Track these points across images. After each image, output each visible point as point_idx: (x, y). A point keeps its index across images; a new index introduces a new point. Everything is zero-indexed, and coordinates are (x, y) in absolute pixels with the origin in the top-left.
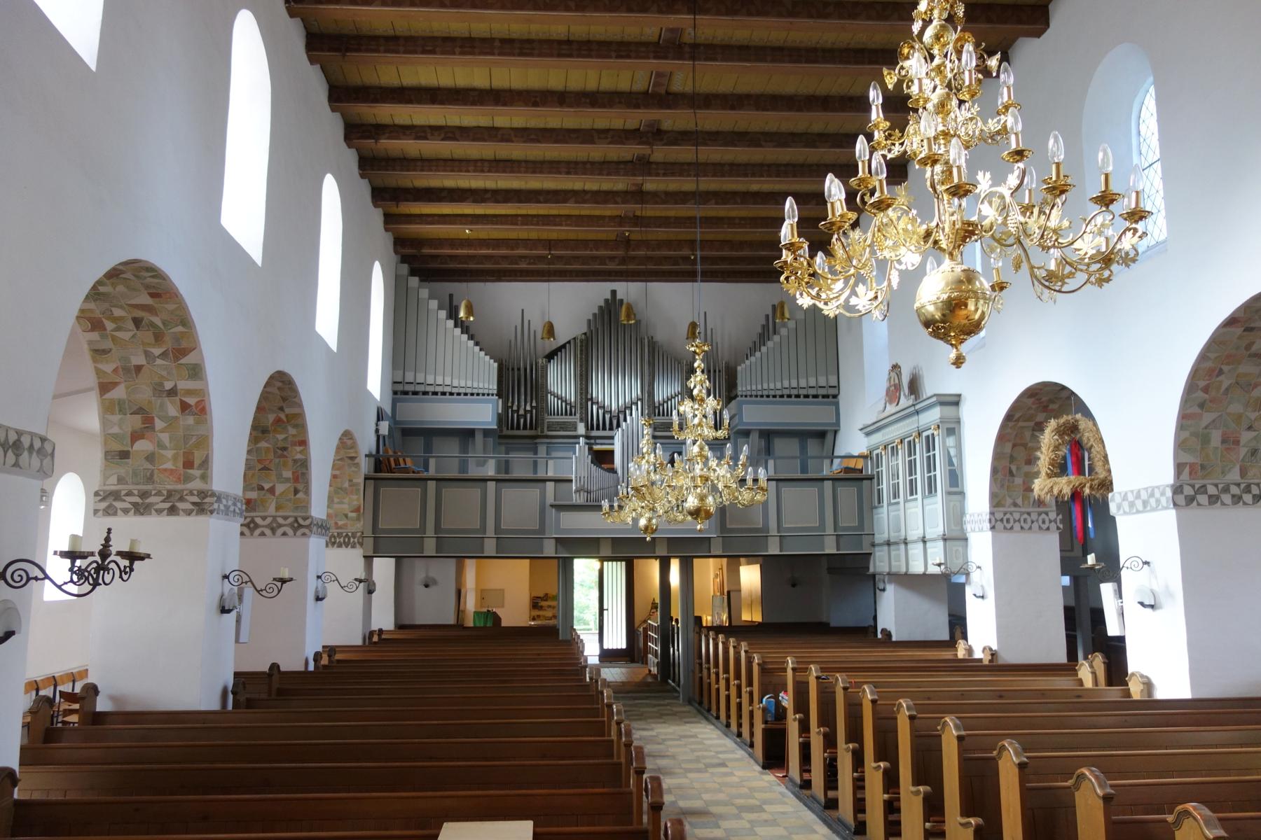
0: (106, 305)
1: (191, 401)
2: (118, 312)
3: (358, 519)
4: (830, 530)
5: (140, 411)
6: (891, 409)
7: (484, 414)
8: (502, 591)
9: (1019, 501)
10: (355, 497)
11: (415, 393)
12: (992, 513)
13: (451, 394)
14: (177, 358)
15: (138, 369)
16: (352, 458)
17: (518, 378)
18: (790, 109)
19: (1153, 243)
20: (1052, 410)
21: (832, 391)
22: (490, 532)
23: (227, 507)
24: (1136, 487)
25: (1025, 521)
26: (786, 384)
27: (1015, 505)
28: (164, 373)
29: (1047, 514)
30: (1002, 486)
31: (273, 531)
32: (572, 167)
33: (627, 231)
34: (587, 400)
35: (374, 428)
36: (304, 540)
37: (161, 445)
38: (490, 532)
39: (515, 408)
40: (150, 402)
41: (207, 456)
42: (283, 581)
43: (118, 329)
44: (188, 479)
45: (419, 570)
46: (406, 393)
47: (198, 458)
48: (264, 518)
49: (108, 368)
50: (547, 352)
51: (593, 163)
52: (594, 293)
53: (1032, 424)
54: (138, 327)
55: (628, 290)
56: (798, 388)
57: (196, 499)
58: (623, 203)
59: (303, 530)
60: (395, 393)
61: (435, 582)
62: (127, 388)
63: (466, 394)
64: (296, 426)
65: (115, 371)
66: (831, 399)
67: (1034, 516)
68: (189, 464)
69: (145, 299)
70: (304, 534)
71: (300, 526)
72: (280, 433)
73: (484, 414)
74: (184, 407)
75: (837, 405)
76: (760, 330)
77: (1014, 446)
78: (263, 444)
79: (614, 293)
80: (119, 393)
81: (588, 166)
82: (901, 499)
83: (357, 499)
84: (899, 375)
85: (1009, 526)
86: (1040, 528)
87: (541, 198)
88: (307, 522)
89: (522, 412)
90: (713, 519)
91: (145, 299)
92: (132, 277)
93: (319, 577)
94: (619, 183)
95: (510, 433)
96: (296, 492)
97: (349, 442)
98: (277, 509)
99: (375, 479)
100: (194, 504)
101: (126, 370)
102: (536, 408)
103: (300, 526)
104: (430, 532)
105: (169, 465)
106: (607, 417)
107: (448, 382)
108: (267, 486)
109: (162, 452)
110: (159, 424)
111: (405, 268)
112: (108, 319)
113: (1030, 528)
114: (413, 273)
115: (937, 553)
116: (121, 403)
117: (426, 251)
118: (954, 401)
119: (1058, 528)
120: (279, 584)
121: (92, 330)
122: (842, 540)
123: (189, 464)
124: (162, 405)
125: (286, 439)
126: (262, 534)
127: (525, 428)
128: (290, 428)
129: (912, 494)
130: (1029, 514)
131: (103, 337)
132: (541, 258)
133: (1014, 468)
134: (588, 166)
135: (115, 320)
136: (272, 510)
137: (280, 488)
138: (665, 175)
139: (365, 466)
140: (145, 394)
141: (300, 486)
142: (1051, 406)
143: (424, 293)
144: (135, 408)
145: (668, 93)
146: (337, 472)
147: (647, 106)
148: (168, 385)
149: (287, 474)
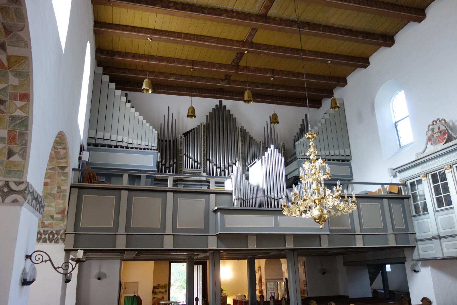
3: (62, 220)
8: (138, 283)
10: (61, 202)
11: (103, 146)
13: (127, 147)
16: (63, 168)
21: (347, 158)
22: (169, 230)
35: (78, 155)
36: (14, 208)
38: (169, 230)
50: (185, 132)
52: (205, 105)
58: (256, 21)
61: (105, 276)
63: (136, 148)
64: (18, 74)
66: (346, 162)
70: (15, 201)
71: (11, 191)
75: (350, 165)
76: (300, 127)
83: (62, 203)
88: (22, 187)
90: (327, 222)
93: (28, 257)
96: (10, 154)
97: (62, 152)
99: (79, 188)
103: (11, 191)
111: (100, 70)
128: (11, 76)
139: (71, 178)
141: (16, 148)
146: (48, 180)
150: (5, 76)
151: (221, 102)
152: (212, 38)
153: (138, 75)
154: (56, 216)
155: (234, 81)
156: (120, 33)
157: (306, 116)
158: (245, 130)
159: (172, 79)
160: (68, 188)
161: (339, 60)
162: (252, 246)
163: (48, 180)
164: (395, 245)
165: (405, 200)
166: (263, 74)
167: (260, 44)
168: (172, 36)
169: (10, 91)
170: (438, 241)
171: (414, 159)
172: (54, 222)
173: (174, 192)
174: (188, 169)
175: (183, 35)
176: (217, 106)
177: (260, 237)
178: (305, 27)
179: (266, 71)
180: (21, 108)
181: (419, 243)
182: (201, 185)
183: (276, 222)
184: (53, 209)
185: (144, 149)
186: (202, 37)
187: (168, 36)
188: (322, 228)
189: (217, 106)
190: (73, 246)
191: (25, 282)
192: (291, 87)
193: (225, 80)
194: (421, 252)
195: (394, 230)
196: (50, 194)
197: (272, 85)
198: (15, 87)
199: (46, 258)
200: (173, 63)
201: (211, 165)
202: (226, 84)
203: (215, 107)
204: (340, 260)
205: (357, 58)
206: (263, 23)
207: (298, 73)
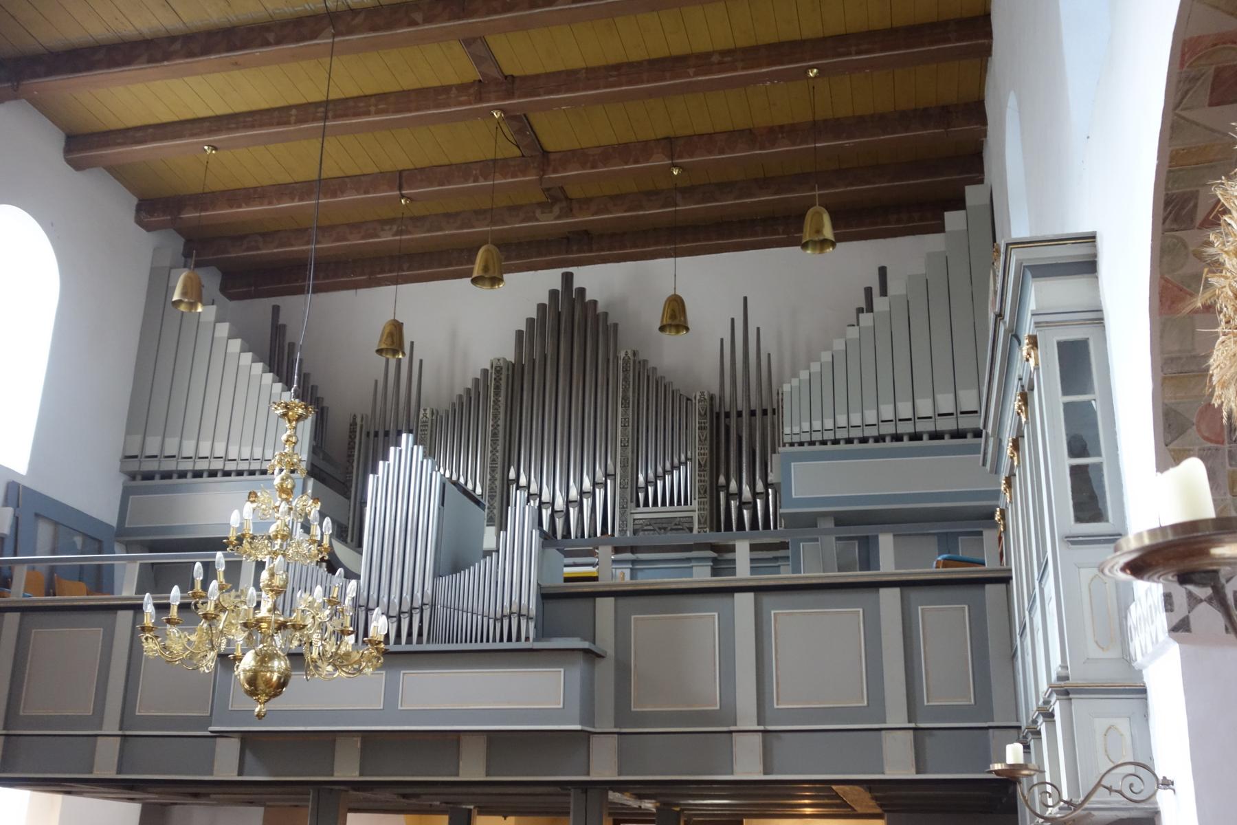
4: (897, 715)
22: (111, 725)
26: (887, 413)
56: (915, 418)
58: (427, 20)
87: (271, 37)
122: (929, 741)
151: (568, 278)
152: (382, 97)
153: (292, 245)
155: (585, 202)
156: (160, 148)
157: (883, 271)
158: (645, 361)
159: (387, 237)
161: (849, 54)
162: (472, 770)
164: (913, 776)
165: (989, 588)
166: (636, 162)
167: (537, 76)
168: (262, 126)
174: (676, 507)
175: (294, 112)
176: (553, 294)
177: (500, 743)
179: (645, 148)
182: (689, 560)
183: (391, 693)
186: (351, 104)
187: (253, 127)
188: (259, 716)
189: (553, 294)
192: (725, 187)
193: (552, 204)
195: (912, 710)
200: (343, 192)
202: (558, 218)
205: (933, 25)
206: (449, 20)
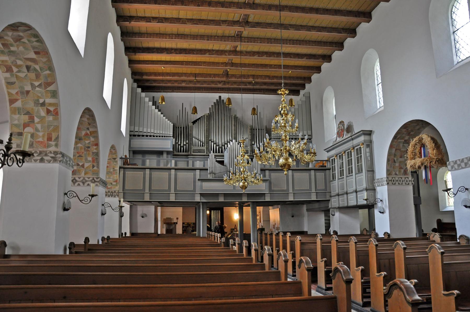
0: (13, 58)
1: (52, 109)
2: (19, 62)
5: (28, 113)
6: (339, 139)
7: (168, 144)
9: (397, 173)
11: (139, 136)
12: (387, 178)
13: (154, 136)
14: (46, 88)
15: (28, 92)
16: (115, 159)
17: (182, 131)
18: (303, 13)
19: (460, 60)
20: (412, 135)
23: (67, 161)
24: (461, 158)
25: (400, 180)
27: (396, 174)
28: (40, 95)
29: (408, 178)
30: (391, 167)
31: (84, 183)
32: (209, 37)
33: (228, 68)
34: (209, 140)
37: (37, 130)
39: (179, 143)
40: (32, 109)
41: (58, 135)
42: (93, 196)
43: (19, 71)
44: (49, 146)
45: (140, 209)
46: (135, 136)
47: (54, 136)
48: (79, 178)
49: (14, 92)
51: (218, 36)
53: (403, 141)
54: (28, 71)
55: (225, 96)
57: (53, 155)
59: (96, 183)
60: (130, 136)
62: (22, 102)
63: (160, 136)
65: (17, 93)
67: (403, 179)
68: (50, 139)
69: (32, 55)
72: (87, 140)
73: (168, 144)
74: (48, 112)
77: (396, 150)
78: (79, 145)
79: (220, 97)
80: (18, 104)
81: (216, 37)
82: (345, 176)
84: (343, 125)
85: (394, 183)
86: (406, 184)
88: (98, 180)
89: (182, 145)
91: (32, 55)
92: (27, 42)
93: (103, 205)
94: (227, 46)
95: (177, 153)
96: (93, 167)
98: (85, 174)
99: (124, 168)
100: (52, 157)
101: (22, 93)
102: (188, 143)
104: (147, 190)
105: (40, 139)
106: (217, 147)
107: (152, 131)
108: (81, 164)
109: (38, 133)
110: (36, 120)
111: (135, 85)
112: (14, 66)
113: (402, 184)
114: (138, 87)
115: (365, 195)
116: (19, 109)
117: (145, 77)
118: (369, 133)
119: (412, 184)
120: (90, 197)
121: (7, 71)
123: (50, 139)
124: (38, 111)
125: (89, 143)
126: (79, 185)
127: (183, 152)
128: (91, 138)
129: (341, 176)
130: (401, 178)
131: (12, 75)
132: (191, 82)
133: (395, 159)
134: (216, 37)
135: (18, 66)
136: (83, 174)
137: (86, 165)
138: (248, 42)
140: (30, 105)
141: (95, 164)
142: (412, 133)
143: (143, 94)
144: (25, 112)
145: (253, 3)
146: (108, 165)
147: (245, 8)
148: (41, 101)
149: (90, 159)
150: (89, 138)
154: (113, 183)
155: (233, 76)
160: (118, 168)
163: (108, 165)
169: (91, 143)
170: (337, 197)
171: (332, 145)
172: (113, 187)
173: (175, 169)
176: (217, 100)
178: (264, 55)
179: (248, 76)
180: (95, 149)
181: (332, 198)
184: (111, 180)
185: (165, 137)
189: (217, 100)
190: (285, 64)
191: (103, 214)
194: (333, 204)
196: (109, 172)
197: (254, 85)
198: (93, 141)
199: (109, 205)
201: (212, 143)
203: (215, 101)
204: (305, 207)
207: (273, 76)
